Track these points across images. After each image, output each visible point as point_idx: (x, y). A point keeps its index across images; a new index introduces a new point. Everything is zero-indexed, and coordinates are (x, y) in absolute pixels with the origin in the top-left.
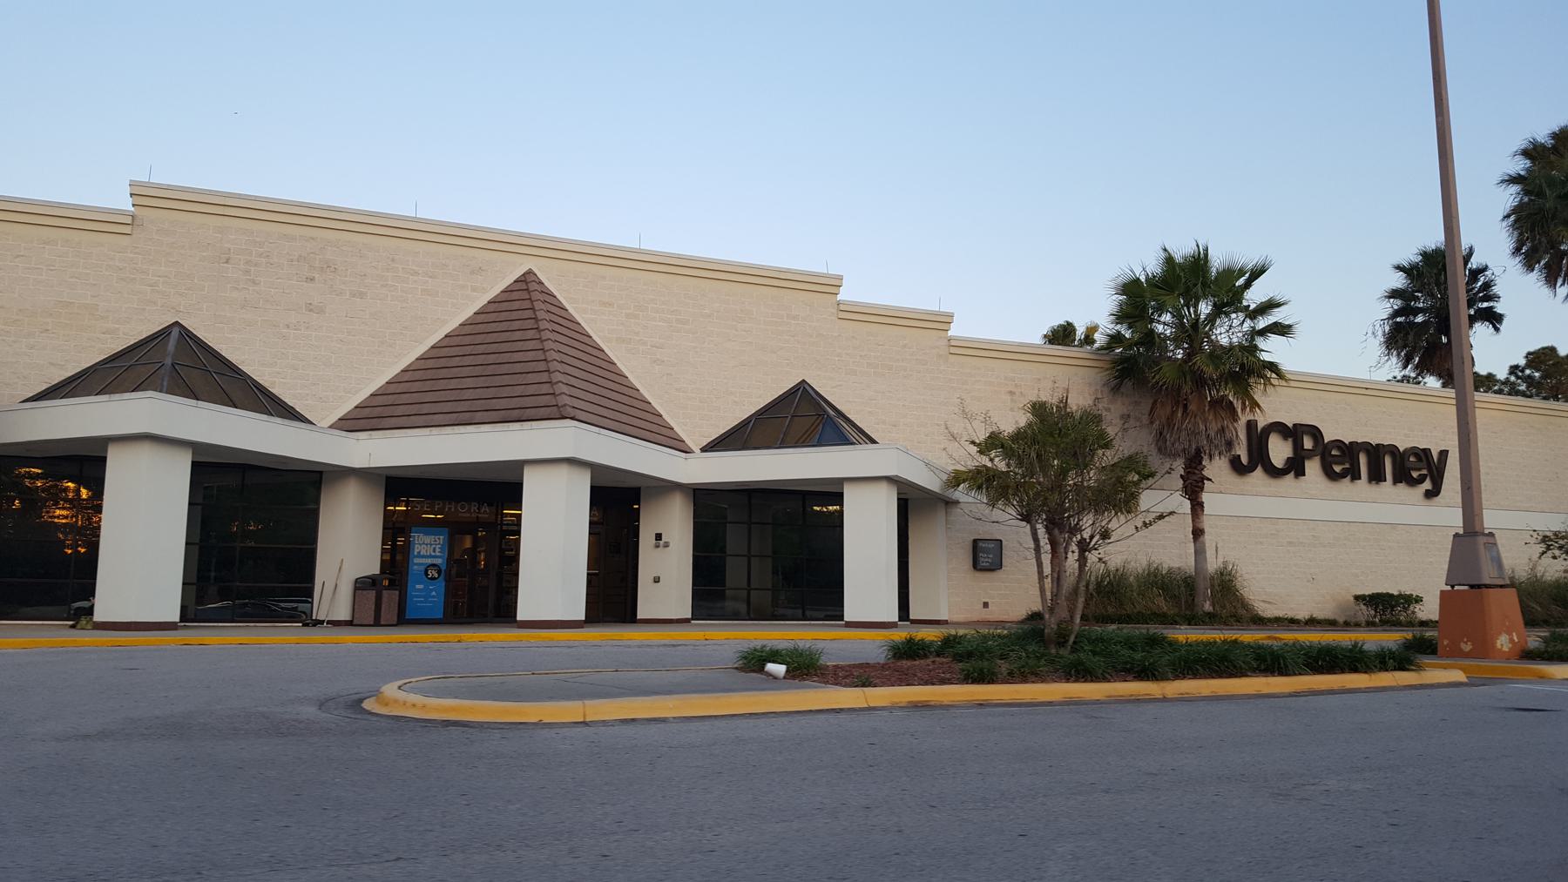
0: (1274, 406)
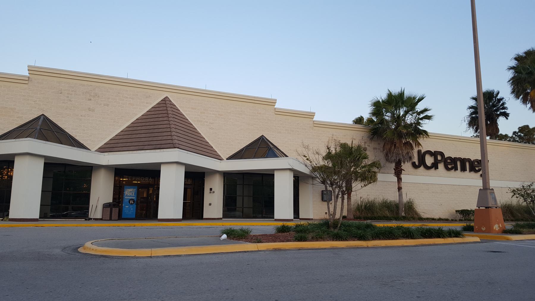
0: (426, 145)
